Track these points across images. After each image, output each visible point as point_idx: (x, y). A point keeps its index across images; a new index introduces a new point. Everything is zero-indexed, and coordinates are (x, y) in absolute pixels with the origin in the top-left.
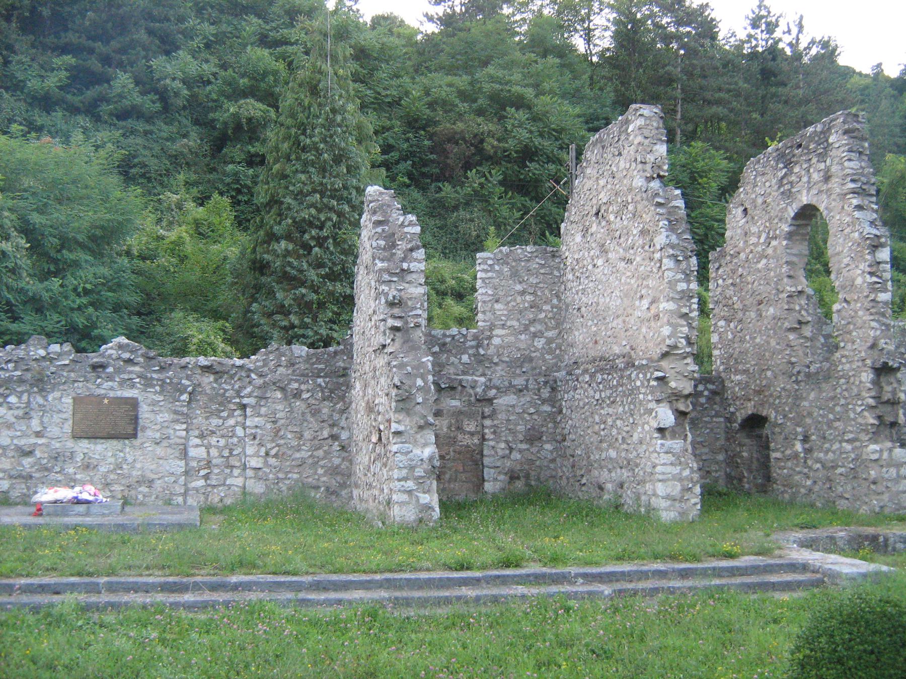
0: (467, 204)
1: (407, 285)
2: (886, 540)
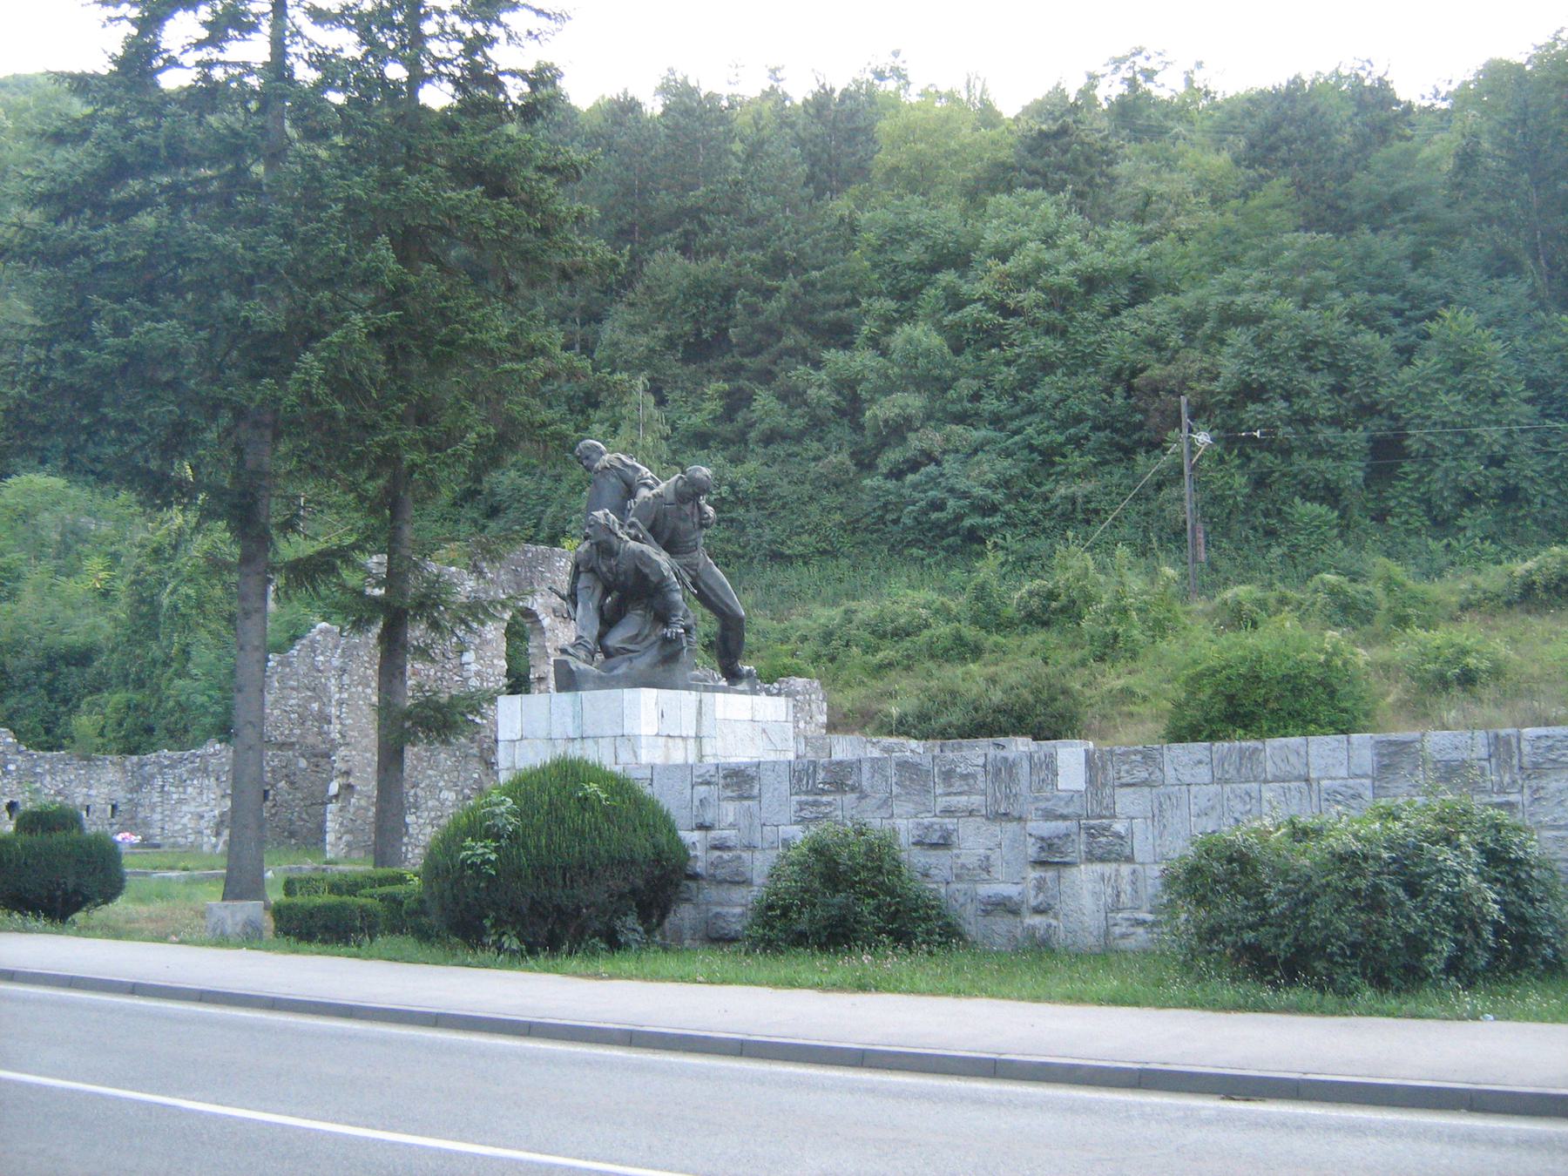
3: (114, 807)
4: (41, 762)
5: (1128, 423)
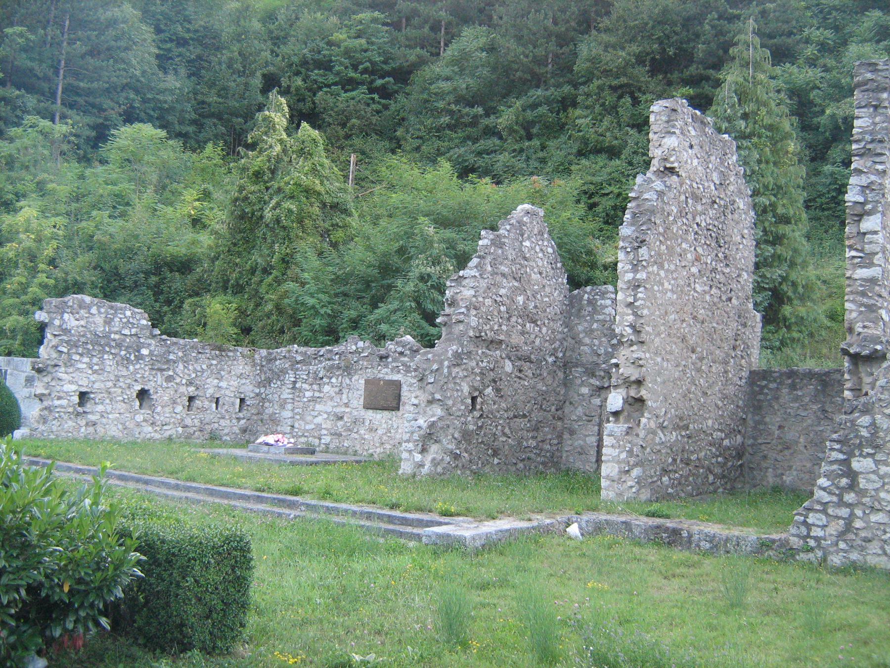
1: (462, 289)
2: (690, 536)
3: (242, 400)
4: (174, 348)
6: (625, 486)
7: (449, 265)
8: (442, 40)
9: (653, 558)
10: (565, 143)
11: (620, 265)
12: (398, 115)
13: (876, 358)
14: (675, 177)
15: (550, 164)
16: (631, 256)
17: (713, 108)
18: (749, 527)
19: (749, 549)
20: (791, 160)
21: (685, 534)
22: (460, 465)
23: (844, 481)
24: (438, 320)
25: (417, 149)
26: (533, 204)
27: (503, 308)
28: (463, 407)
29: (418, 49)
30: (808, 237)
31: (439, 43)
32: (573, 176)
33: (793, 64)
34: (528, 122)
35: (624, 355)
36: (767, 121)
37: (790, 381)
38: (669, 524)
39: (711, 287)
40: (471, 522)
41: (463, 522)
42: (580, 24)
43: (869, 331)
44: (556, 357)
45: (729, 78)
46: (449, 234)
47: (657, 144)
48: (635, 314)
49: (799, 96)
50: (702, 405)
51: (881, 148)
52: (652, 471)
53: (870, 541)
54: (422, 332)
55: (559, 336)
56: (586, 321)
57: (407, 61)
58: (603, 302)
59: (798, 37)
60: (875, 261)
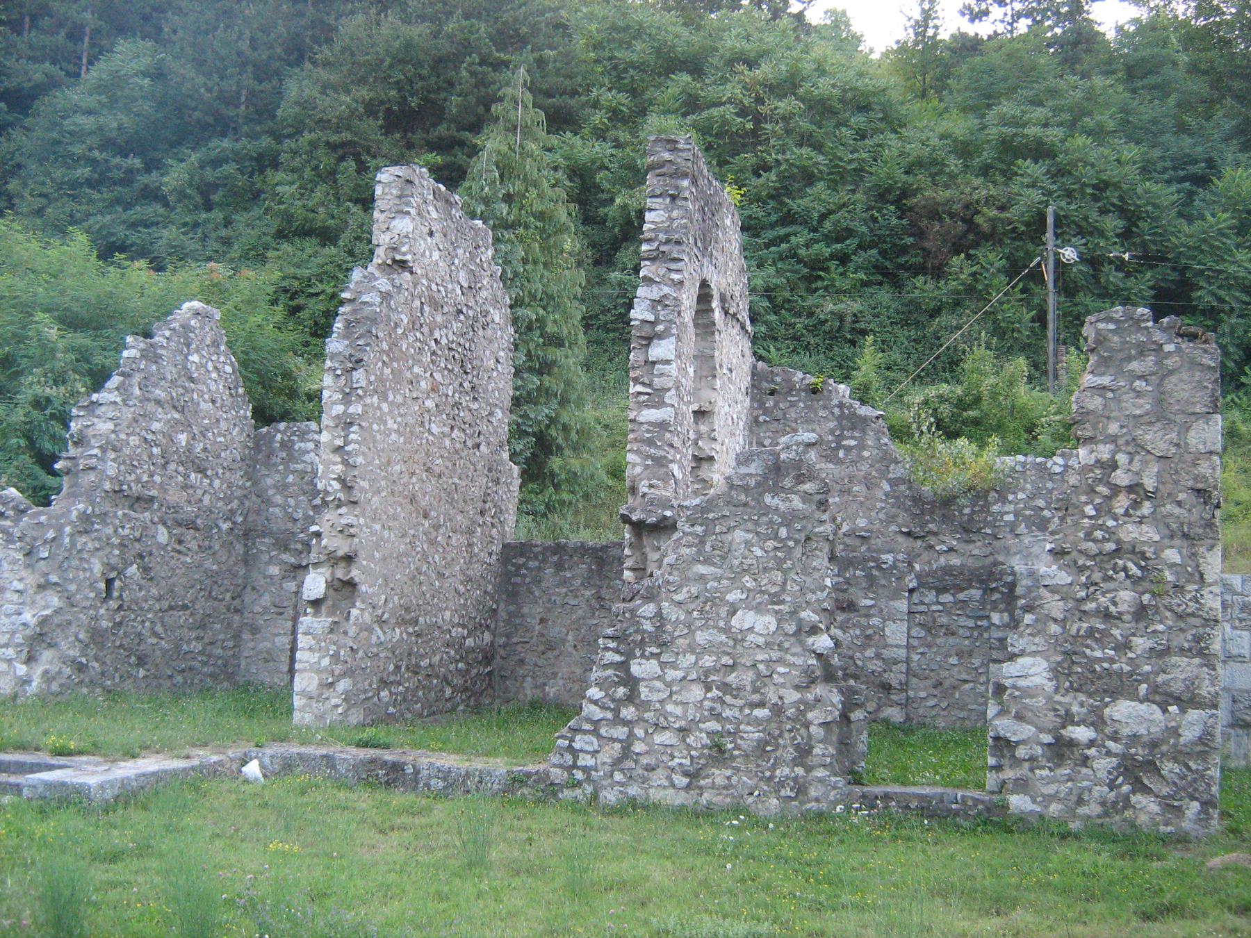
0: (957, 304)
1: (96, 420)
2: (417, 772)
5: (895, 245)
6: (328, 705)
7: (79, 385)
8: (85, 54)
9: (364, 805)
10: (259, 219)
11: (326, 394)
12: (11, 159)
13: (664, 527)
14: (407, 274)
15: (236, 247)
16: (342, 381)
17: (466, 184)
18: (496, 756)
19: (496, 787)
20: (567, 262)
21: (409, 770)
22: (87, 680)
23: (621, 691)
24: (57, 466)
25: (39, 212)
26: (208, 303)
27: (156, 451)
28: (92, 595)
29: (47, 64)
30: (587, 367)
31: (80, 59)
32: (268, 266)
33: (576, 134)
34: (208, 184)
35: (328, 521)
36: (538, 207)
37: (556, 558)
38: (388, 756)
39: (452, 428)
40: (97, 764)
41: (87, 763)
42: (288, 51)
43: (657, 492)
44: (234, 523)
45: (489, 145)
46: (80, 339)
47: (384, 227)
48: (345, 463)
49: (581, 176)
50: (436, 590)
51: (679, 252)
52: (366, 683)
53: (654, 769)
54: (35, 483)
55: (239, 493)
56: (278, 471)
57: (30, 80)
58: (302, 445)
59: (584, 99)
60: (666, 400)
